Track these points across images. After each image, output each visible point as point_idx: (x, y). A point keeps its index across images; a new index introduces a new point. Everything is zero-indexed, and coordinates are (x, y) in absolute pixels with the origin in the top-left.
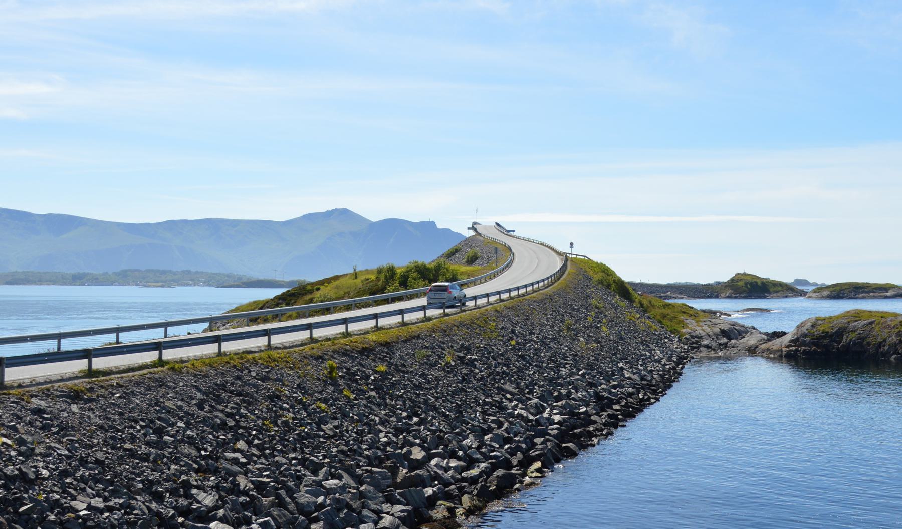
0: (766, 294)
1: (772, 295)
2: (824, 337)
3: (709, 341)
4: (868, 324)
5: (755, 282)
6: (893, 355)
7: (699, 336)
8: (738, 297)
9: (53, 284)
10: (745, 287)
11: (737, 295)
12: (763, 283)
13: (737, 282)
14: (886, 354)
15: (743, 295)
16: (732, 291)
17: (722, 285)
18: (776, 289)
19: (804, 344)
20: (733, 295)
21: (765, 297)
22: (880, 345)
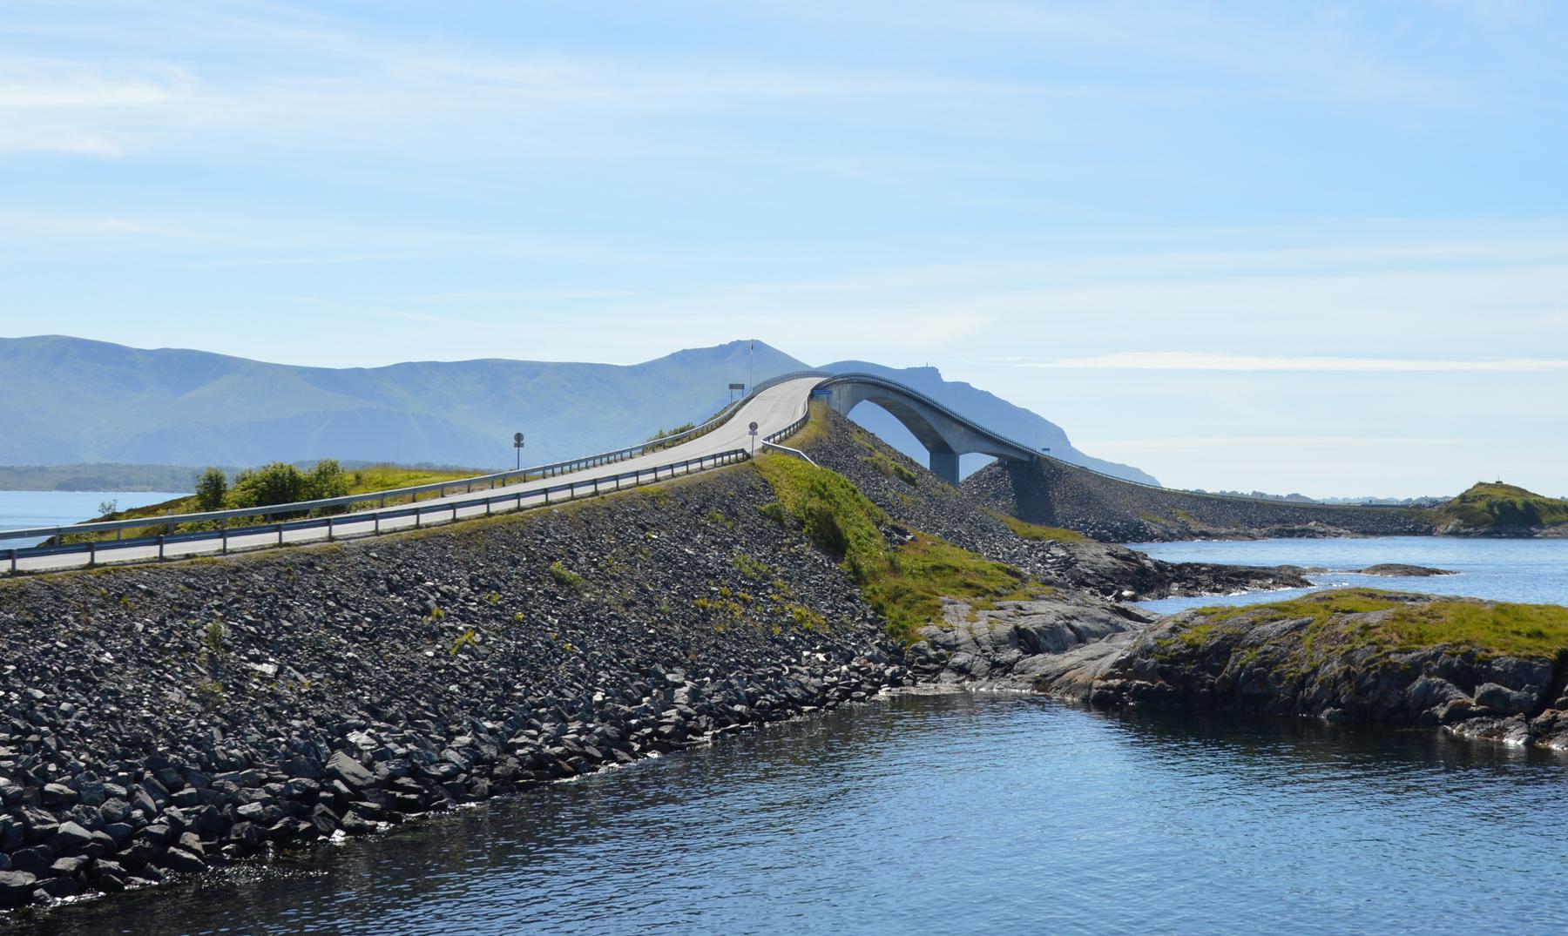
0: (1533, 529)
1: (1545, 531)
2: (1187, 658)
3: (971, 656)
4: (1292, 630)
5: (1509, 502)
6: (1325, 707)
7: (953, 643)
8: (1471, 533)
9: (153, 490)
10: (1489, 512)
11: (1471, 529)
12: (1527, 505)
13: (1474, 501)
14: (1312, 705)
15: (1482, 530)
16: (1461, 521)
17: (1440, 509)
18: (1557, 517)
19: (1141, 672)
20: (1463, 530)
21: (1530, 536)
22: (1303, 681)
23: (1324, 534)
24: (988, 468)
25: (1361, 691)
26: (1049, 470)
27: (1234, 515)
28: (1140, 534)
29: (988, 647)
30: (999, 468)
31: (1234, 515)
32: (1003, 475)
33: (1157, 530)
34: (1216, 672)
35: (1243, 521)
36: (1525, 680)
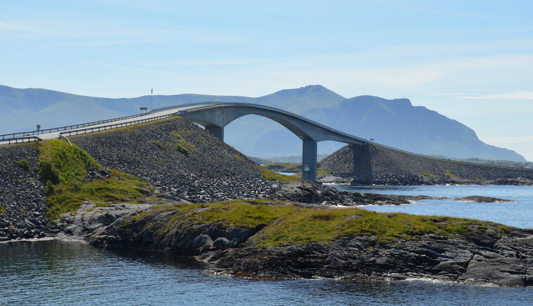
14: (162, 246)
22: (163, 236)
23: (523, 184)
24: (343, 148)
25: (178, 241)
26: (372, 150)
27: (481, 173)
28: (415, 181)
29: (87, 222)
30: (348, 148)
31: (481, 173)
32: (350, 151)
33: (426, 179)
34: (137, 232)
35: (485, 176)
36: (235, 236)
